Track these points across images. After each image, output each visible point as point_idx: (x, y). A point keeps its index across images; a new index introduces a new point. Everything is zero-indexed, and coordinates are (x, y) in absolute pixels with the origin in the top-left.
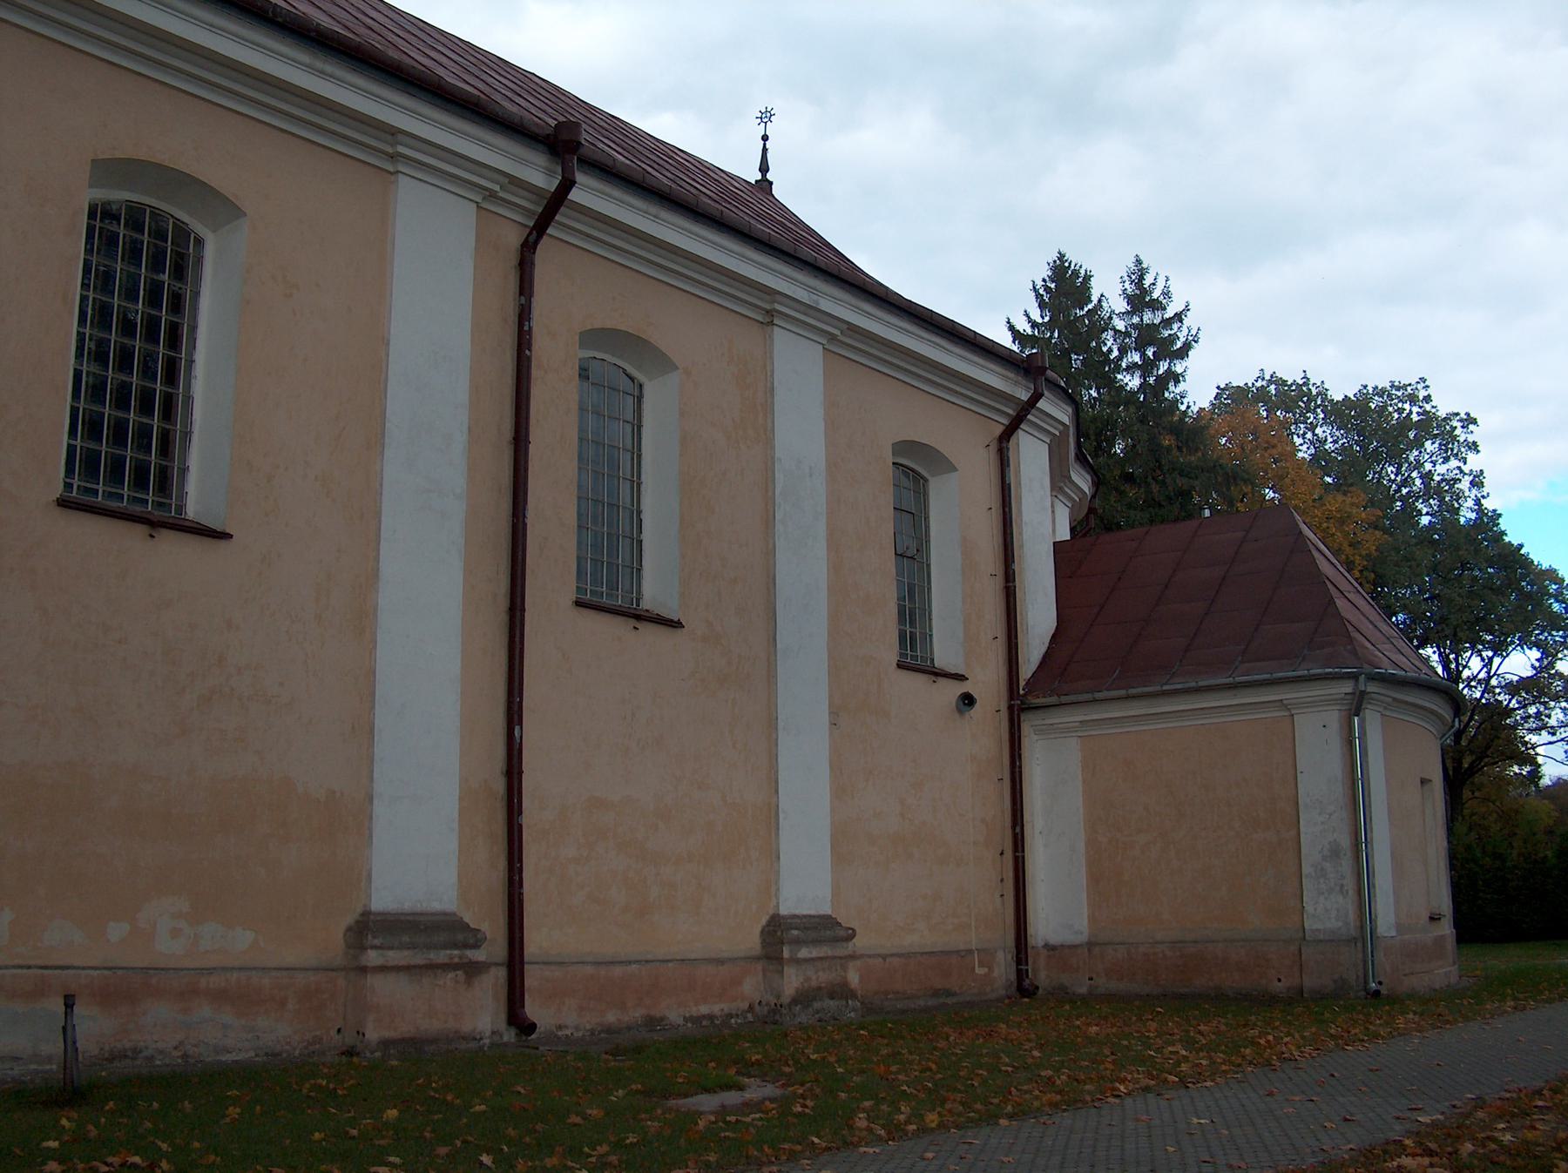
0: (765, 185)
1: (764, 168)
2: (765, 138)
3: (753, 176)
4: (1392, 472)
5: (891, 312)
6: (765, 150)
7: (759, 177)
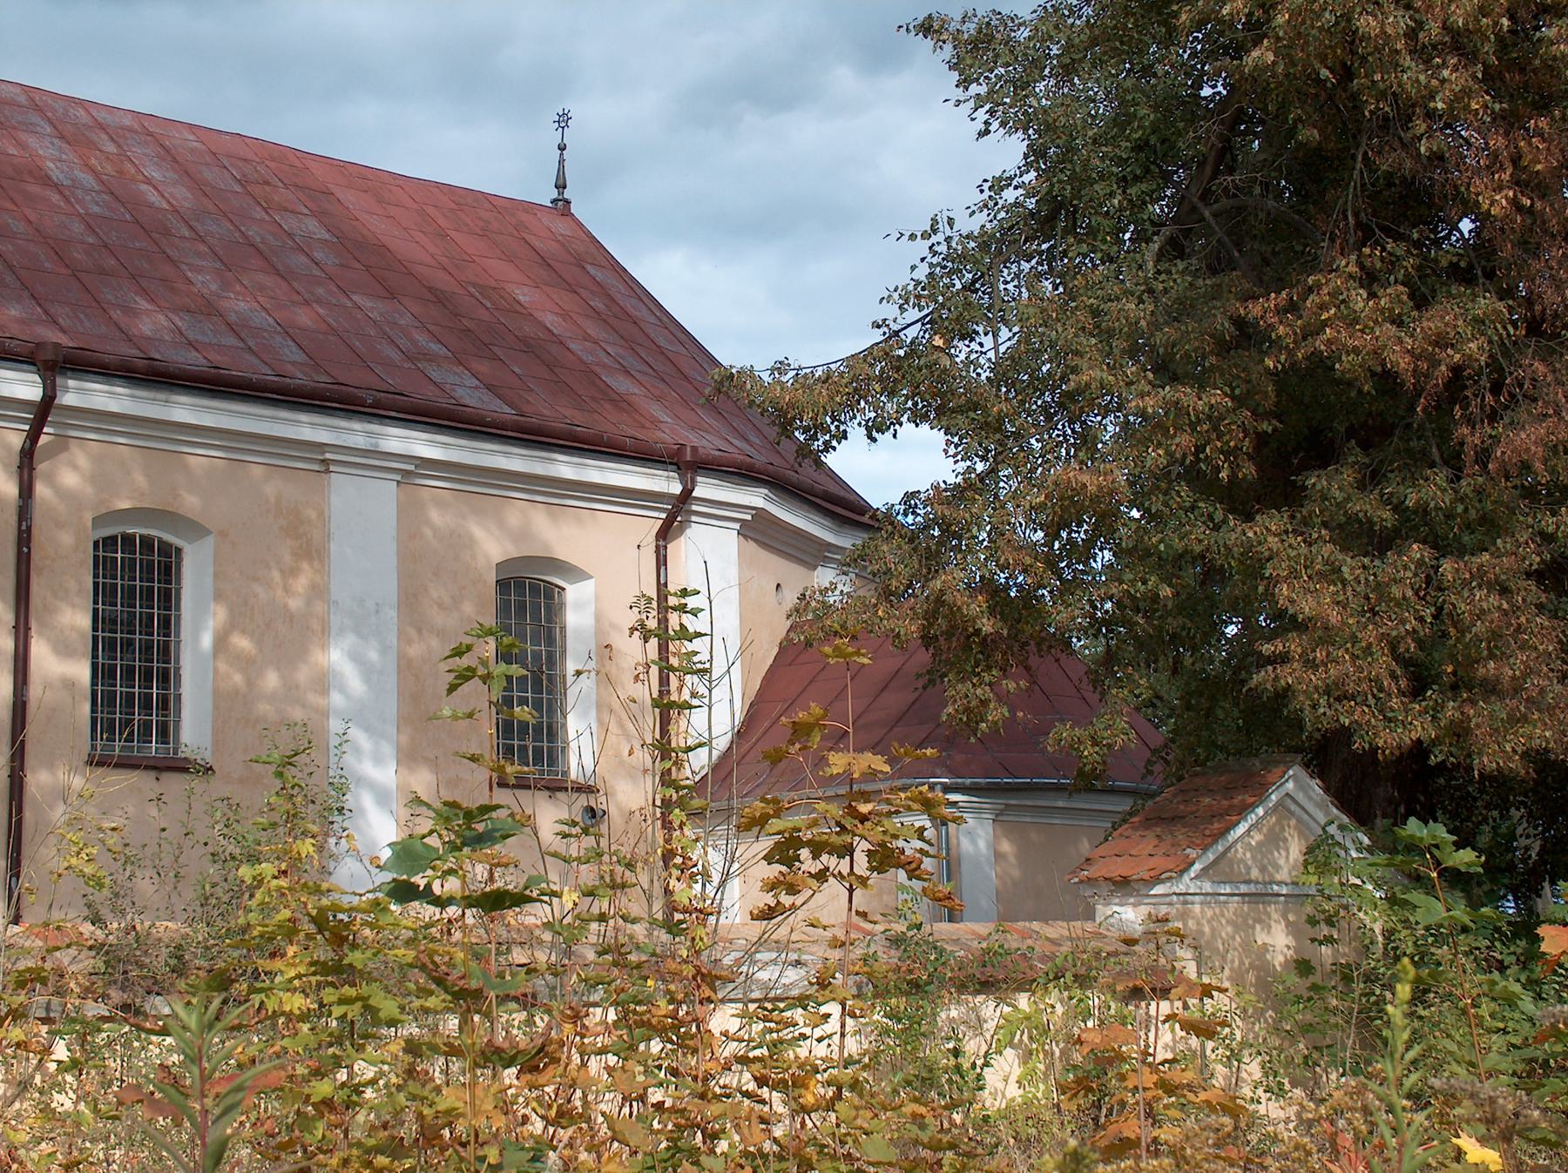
0: (562, 206)
1: (561, 186)
2: (562, 148)
3: (544, 195)
4: (1492, 622)
5: (483, 440)
6: (561, 162)
7: (554, 194)
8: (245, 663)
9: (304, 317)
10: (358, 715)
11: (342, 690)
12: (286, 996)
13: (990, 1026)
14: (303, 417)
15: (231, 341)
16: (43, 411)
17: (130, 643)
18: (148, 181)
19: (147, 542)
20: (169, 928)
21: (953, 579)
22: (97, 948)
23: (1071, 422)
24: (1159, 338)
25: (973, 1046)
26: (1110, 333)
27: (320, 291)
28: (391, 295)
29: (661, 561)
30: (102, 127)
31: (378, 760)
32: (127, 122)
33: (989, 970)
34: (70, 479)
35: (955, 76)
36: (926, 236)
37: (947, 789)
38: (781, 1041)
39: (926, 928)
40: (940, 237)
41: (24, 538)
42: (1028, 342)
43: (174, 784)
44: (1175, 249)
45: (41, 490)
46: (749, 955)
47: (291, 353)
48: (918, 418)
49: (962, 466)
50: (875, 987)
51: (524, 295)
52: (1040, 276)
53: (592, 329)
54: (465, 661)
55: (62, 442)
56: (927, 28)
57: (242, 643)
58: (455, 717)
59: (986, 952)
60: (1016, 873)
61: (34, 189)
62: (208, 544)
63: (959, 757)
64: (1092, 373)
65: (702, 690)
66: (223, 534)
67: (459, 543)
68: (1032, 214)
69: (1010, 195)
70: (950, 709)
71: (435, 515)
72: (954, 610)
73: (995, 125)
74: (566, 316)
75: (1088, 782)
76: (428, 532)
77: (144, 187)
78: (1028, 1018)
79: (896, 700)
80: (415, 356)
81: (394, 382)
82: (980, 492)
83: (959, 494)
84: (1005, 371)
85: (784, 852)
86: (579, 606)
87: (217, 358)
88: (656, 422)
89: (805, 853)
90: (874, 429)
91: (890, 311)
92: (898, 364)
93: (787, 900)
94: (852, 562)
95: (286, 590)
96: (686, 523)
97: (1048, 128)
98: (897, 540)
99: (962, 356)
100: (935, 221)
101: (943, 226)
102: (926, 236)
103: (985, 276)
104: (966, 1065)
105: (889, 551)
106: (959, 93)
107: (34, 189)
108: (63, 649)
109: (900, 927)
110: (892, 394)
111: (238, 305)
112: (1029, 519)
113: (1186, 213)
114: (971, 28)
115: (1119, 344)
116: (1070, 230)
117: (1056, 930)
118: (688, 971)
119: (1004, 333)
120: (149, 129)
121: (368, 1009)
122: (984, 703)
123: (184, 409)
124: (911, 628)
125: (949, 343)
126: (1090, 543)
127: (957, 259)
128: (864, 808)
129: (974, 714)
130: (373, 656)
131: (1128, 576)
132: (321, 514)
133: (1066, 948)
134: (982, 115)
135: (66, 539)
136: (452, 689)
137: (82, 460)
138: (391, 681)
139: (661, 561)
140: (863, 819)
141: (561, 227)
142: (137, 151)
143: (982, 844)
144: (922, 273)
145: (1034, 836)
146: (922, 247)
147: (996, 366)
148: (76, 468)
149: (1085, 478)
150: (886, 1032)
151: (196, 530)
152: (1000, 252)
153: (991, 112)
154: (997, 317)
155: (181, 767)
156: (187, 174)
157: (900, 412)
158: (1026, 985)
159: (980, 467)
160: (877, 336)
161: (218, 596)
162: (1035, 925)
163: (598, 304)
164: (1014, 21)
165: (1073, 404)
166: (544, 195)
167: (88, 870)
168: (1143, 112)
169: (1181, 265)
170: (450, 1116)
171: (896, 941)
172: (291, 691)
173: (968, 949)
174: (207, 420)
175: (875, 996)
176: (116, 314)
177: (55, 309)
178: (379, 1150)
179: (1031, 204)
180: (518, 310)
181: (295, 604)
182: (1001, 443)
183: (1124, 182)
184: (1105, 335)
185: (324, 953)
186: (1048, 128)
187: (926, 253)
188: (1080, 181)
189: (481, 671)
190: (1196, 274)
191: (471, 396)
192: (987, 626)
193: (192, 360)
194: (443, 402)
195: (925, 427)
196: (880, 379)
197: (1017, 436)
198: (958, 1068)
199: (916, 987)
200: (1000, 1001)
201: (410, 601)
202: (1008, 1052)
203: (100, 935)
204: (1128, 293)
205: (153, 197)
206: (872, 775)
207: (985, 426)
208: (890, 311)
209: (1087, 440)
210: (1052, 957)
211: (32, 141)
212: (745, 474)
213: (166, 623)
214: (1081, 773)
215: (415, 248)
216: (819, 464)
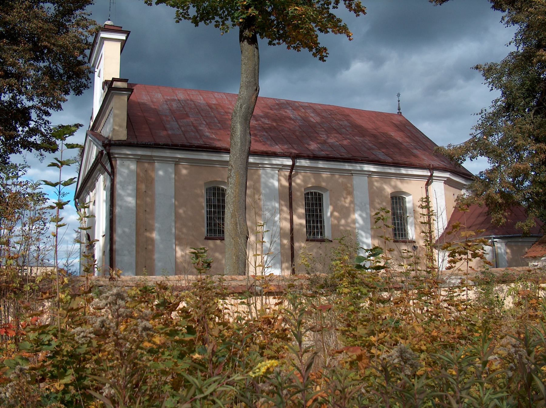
0: (400, 114)
1: (399, 109)
2: (399, 101)
6: (399, 104)
7: (398, 111)
8: (336, 218)
9: (345, 142)
10: (362, 228)
11: (358, 223)
12: (344, 289)
13: (505, 291)
14: (346, 164)
15: (330, 149)
16: (293, 167)
17: (313, 215)
18: (311, 117)
19: (315, 193)
20: (323, 275)
21: (493, 190)
22: (309, 279)
23: (517, 153)
24: (535, 133)
25: (501, 295)
26: (524, 133)
27: (348, 136)
28: (363, 136)
29: (427, 190)
30: (301, 106)
31: (367, 238)
32: (306, 105)
33: (504, 278)
34: (298, 181)
35: (484, 78)
36: (480, 114)
37: (494, 238)
38: (453, 296)
39: (490, 270)
40: (483, 114)
41: (290, 194)
42: (505, 136)
43: (324, 244)
44: (537, 113)
45: (293, 184)
46: (449, 277)
47: (343, 150)
48: (481, 155)
49: (492, 165)
50: (477, 282)
51: (393, 134)
52: (507, 120)
53: (408, 140)
54: (379, 216)
55: (297, 173)
56: (477, 68)
57: (336, 214)
58: (377, 228)
59: (503, 274)
60: (511, 257)
61: (288, 121)
62: (328, 192)
63: (497, 231)
64: (520, 142)
65: (435, 219)
66: (331, 191)
67: (381, 190)
68: (504, 107)
69: (499, 103)
70: (493, 220)
71: (376, 184)
72: (492, 198)
73: (494, 88)
74: (402, 138)
75: (525, 235)
76: (375, 188)
77: (310, 118)
78: (514, 289)
79: (482, 219)
80: (370, 149)
81: (366, 155)
82: (497, 170)
83: (492, 171)
84: (500, 143)
85: (452, 255)
86: (409, 202)
87: (328, 153)
88: (423, 159)
89: (457, 254)
90: (472, 158)
91: (473, 131)
92: (476, 143)
93: (453, 265)
94: (468, 188)
95: (345, 202)
96: (432, 182)
97: (506, 87)
98: (478, 182)
99: (491, 140)
100: (482, 110)
101: (484, 111)
102: (480, 114)
103: (494, 122)
104: (500, 300)
105: (477, 185)
106: (485, 81)
107: (288, 121)
108: (299, 217)
109: (484, 270)
110: (475, 150)
111: (331, 141)
112: (508, 176)
113: (539, 104)
114: (487, 67)
115: (526, 135)
116: (513, 110)
117: (520, 269)
118: (432, 281)
119: (500, 134)
120: (310, 107)
121: (360, 291)
122: (501, 218)
123: (321, 164)
124: (483, 202)
125: (487, 137)
126: (523, 180)
127: (488, 119)
128: (470, 244)
129: (498, 221)
130: (364, 215)
131: (532, 187)
132: (351, 185)
133: (522, 273)
134: (491, 86)
135: (298, 194)
136: (376, 222)
137: (301, 177)
138: (369, 220)
139: (427, 190)
140: (469, 246)
141: (400, 118)
142: (308, 111)
143: (503, 251)
144: (480, 122)
145: (515, 248)
146: (479, 116)
147: (498, 142)
148: (299, 178)
149: (520, 166)
150: (481, 293)
151: (325, 190)
152: (497, 116)
153: (493, 85)
154: (498, 130)
155: (322, 241)
156: (318, 114)
157: (477, 154)
158: (513, 281)
159: (497, 165)
160: (471, 137)
161: (331, 204)
162: (515, 268)
163: (409, 135)
164: (496, 65)
165: (517, 149)
166: (396, 112)
167: (306, 263)
168: (528, 82)
169: (539, 116)
170: (379, 314)
171: (483, 273)
172: (347, 224)
173: (499, 274)
174: (326, 166)
175: (479, 285)
176: (306, 146)
177: (294, 145)
178: (365, 321)
179: (504, 105)
180: (390, 137)
181: (347, 205)
182: (500, 159)
183: (524, 98)
184: (523, 133)
185: (350, 279)
186: (506, 87)
187: (480, 117)
188: (514, 99)
189: (382, 218)
190: (543, 118)
191: (382, 156)
192: (500, 201)
193: (323, 153)
194: (376, 159)
195: (483, 157)
196: (472, 147)
197: (504, 157)
198: (498, 301)
199: (488, 283)
200: (507, 285)
201: (372, 203)
202: (510, 296)
203: (309, 277)
204: (527, 123)
205: (312, 120)
206: (471, 236)
207: (497, 156)
208: (473, 131)
209: (520, 158)
210: (519, 275)
211: (288, 111)
212: (444, 170)
213: (320, 210)
214: (524, 233)
215: (368, 125)
216: (460, 165)
